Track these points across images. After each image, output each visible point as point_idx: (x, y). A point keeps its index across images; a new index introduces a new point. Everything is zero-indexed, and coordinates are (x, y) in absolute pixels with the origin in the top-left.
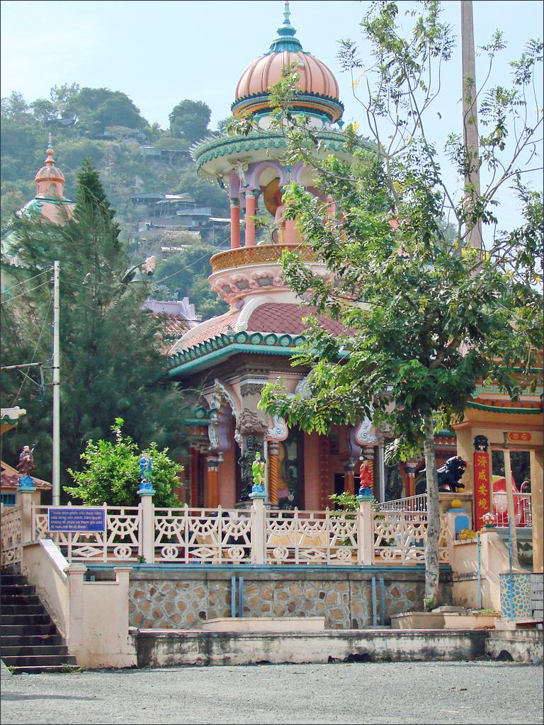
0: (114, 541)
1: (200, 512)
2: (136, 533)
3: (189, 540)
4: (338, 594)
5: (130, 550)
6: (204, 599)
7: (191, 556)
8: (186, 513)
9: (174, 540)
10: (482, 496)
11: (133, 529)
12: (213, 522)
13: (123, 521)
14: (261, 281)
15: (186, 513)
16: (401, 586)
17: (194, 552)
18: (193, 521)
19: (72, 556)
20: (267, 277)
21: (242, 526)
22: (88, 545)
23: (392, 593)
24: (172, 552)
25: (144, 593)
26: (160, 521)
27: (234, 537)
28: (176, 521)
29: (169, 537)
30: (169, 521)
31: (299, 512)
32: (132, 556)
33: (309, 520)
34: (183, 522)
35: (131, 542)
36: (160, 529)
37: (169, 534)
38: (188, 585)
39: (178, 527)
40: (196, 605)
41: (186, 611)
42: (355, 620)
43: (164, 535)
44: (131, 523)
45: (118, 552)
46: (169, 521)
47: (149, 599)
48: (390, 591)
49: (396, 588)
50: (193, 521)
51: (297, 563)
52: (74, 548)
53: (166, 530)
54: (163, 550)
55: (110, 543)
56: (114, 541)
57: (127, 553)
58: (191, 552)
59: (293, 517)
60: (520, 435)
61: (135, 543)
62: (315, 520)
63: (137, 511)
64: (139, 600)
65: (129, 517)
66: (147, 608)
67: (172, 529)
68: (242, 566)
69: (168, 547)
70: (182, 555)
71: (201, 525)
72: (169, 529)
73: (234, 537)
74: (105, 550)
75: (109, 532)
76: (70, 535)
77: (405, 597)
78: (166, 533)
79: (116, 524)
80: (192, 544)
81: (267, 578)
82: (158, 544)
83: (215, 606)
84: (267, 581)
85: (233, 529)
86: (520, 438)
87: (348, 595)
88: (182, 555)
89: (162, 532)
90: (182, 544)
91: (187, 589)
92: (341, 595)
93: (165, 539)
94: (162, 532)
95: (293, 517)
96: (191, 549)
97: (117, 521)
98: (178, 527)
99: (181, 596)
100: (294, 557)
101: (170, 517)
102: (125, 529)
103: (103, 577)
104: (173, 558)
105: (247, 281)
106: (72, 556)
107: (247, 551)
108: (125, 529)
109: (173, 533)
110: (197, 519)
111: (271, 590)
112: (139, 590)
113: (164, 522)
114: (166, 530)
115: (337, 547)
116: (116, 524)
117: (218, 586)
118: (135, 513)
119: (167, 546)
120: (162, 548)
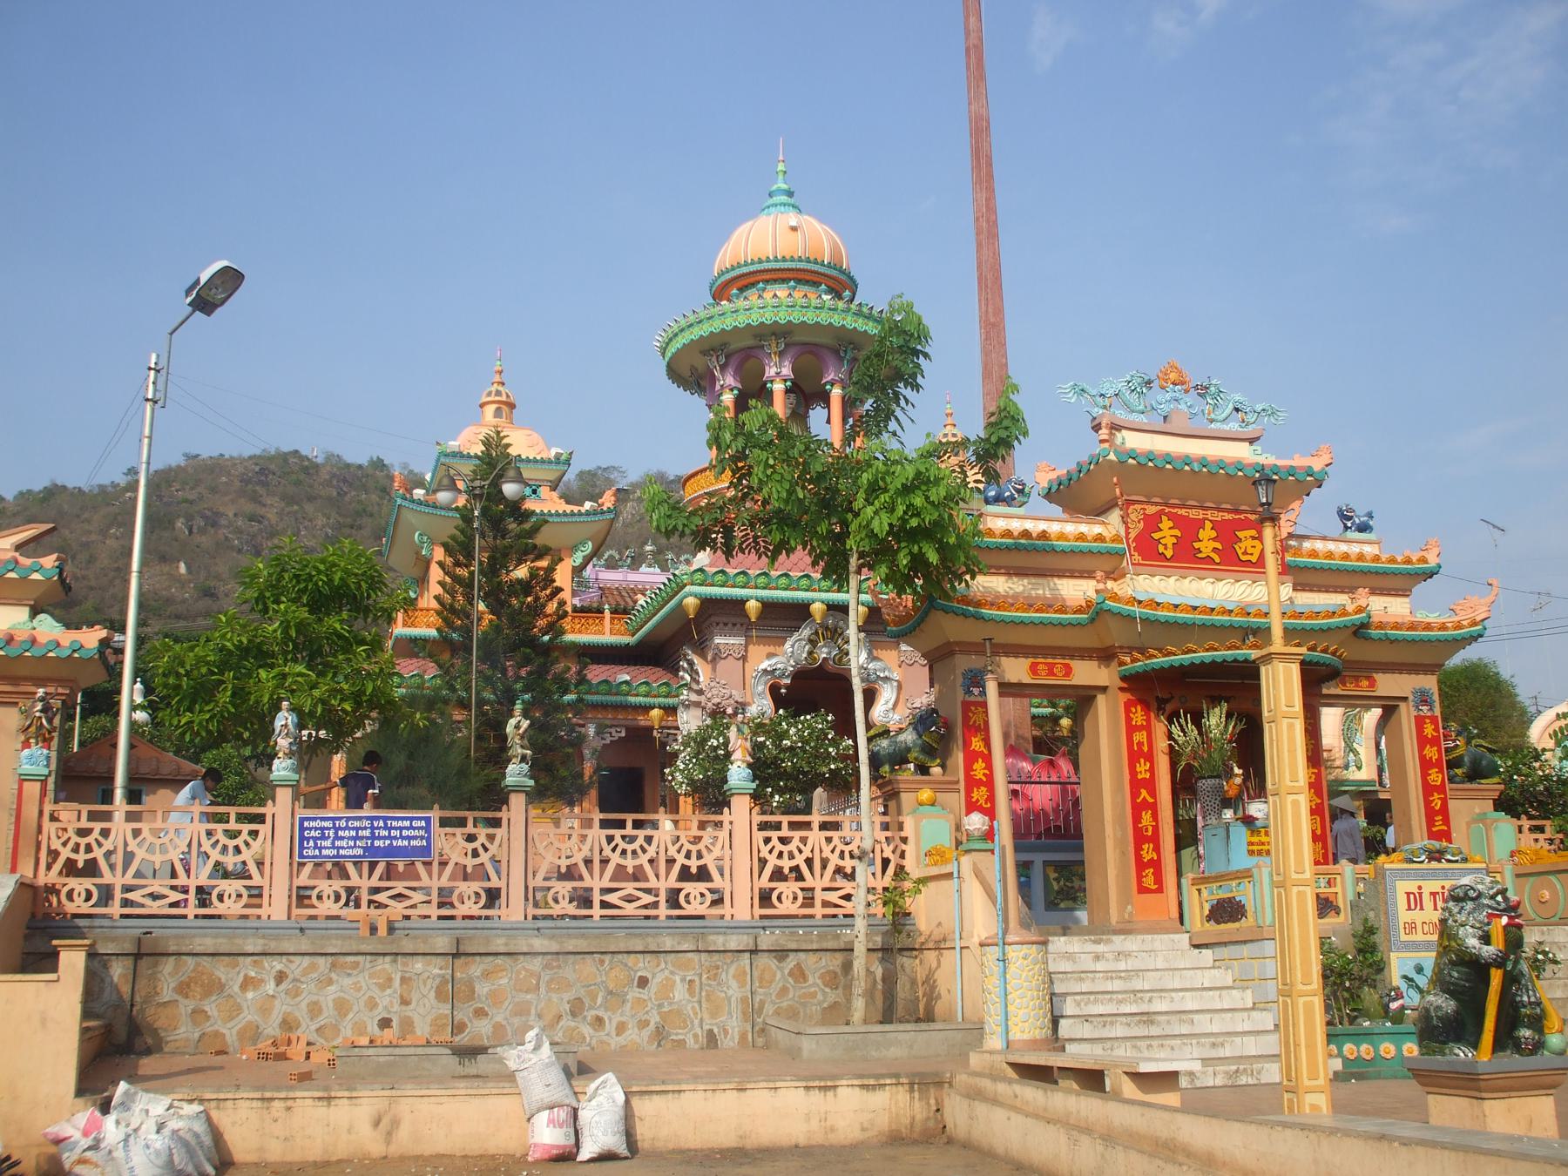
0: (771, 880)
1: (625, 821)
2: (495, 861)
3: (813, 875)
4: (677, 978)
5: (800, 895)
6: (389, 991)
7: (604, 905)
8: (816, 826)
9: (91, 869)
10: (979, 783)
11: (804, 856)
12: (804, 840)
13: (233, 835)
15: (816, 826)
16: (809, 961)
17: (612, 898)
18: (829, 840)
19: (602, 907)
21: (641, 847)
22: (630, 888)
23: (791, 974)
24: (332, 898)
25: (262, 981)
26: (829, 840)
27: (465, 866)
28: (245, 833)
29: (694, 870)
30: (783, 841)
31: (602, 816)
32: (803, 906)
33: (623, 832)
34: (589, 839)
35: (250, 877)
36: (768, 856)
37: (786, 864)
38: (357, 963)
39: (800, 851)
40: (372, 1004)
41: (351, 1015)
42: (710, 1032)
43: (68, 859)
44: (802, 846)
45: (779, 898)
46: (783, 841)
47: (271, 992)
48: (786, 972)
49: (798, 966)
50: (767, 840)
51: (819, 916)
52: (376, 890)
53: (688, 856)
54: (800, 900)
55: (672, 882)
56: (771, 880)
57: (795, 898)
58: (130, 896)
59: (500, 826)
60: (1051, 673)
61: (257, 880)
62: (635, 832)
63: (264, 815)
64: (250, 995)
65: (246, 828)
66: (265, 1011)
67: (89, 849)
68: (242, 923)
69: (788, 888)
70: (809, 902)
71: (79, 840)
72: (694, 855)
73: (465, 866)
74: (662, 898)
75: (54, 854)
76: (366, 868)
77: (819, 982)
78: (687, 862)
79: (218, 841)
80: (129, 879)
81: (525, 950)
82: (764, 881)
83: (412, 1007)
84: (525, 954)
85: (842, 852)
86: (1051, 673)
87: (697, 982)
88: (809, 902)
89: (773, 861)
90: (108, 879)
91: (355, 972)
92: (683, 980)
93: (778, 875)
94: (773, 861)
95: (500, 826)
96: (128, 889)
97: (775, 842)
98: (800, 851)
99: (342, 985)
100: (812, 905)
101: (629, 830)
102: (791, 856)
103: (173, 949)
104: (475, 910)
106: (602, 907)
107: (256, 894)
108: (700, 856)
109: (701, 862)
110: (774, 835)
111: (532, 974)
112: (253, 974)
113: (775, 842)
114: (688, 856)
115: (773, 885)
116: (218, 841)
117: (418, 965)
118: (260, 819)
119: (781, 886)
120: (680, 890)
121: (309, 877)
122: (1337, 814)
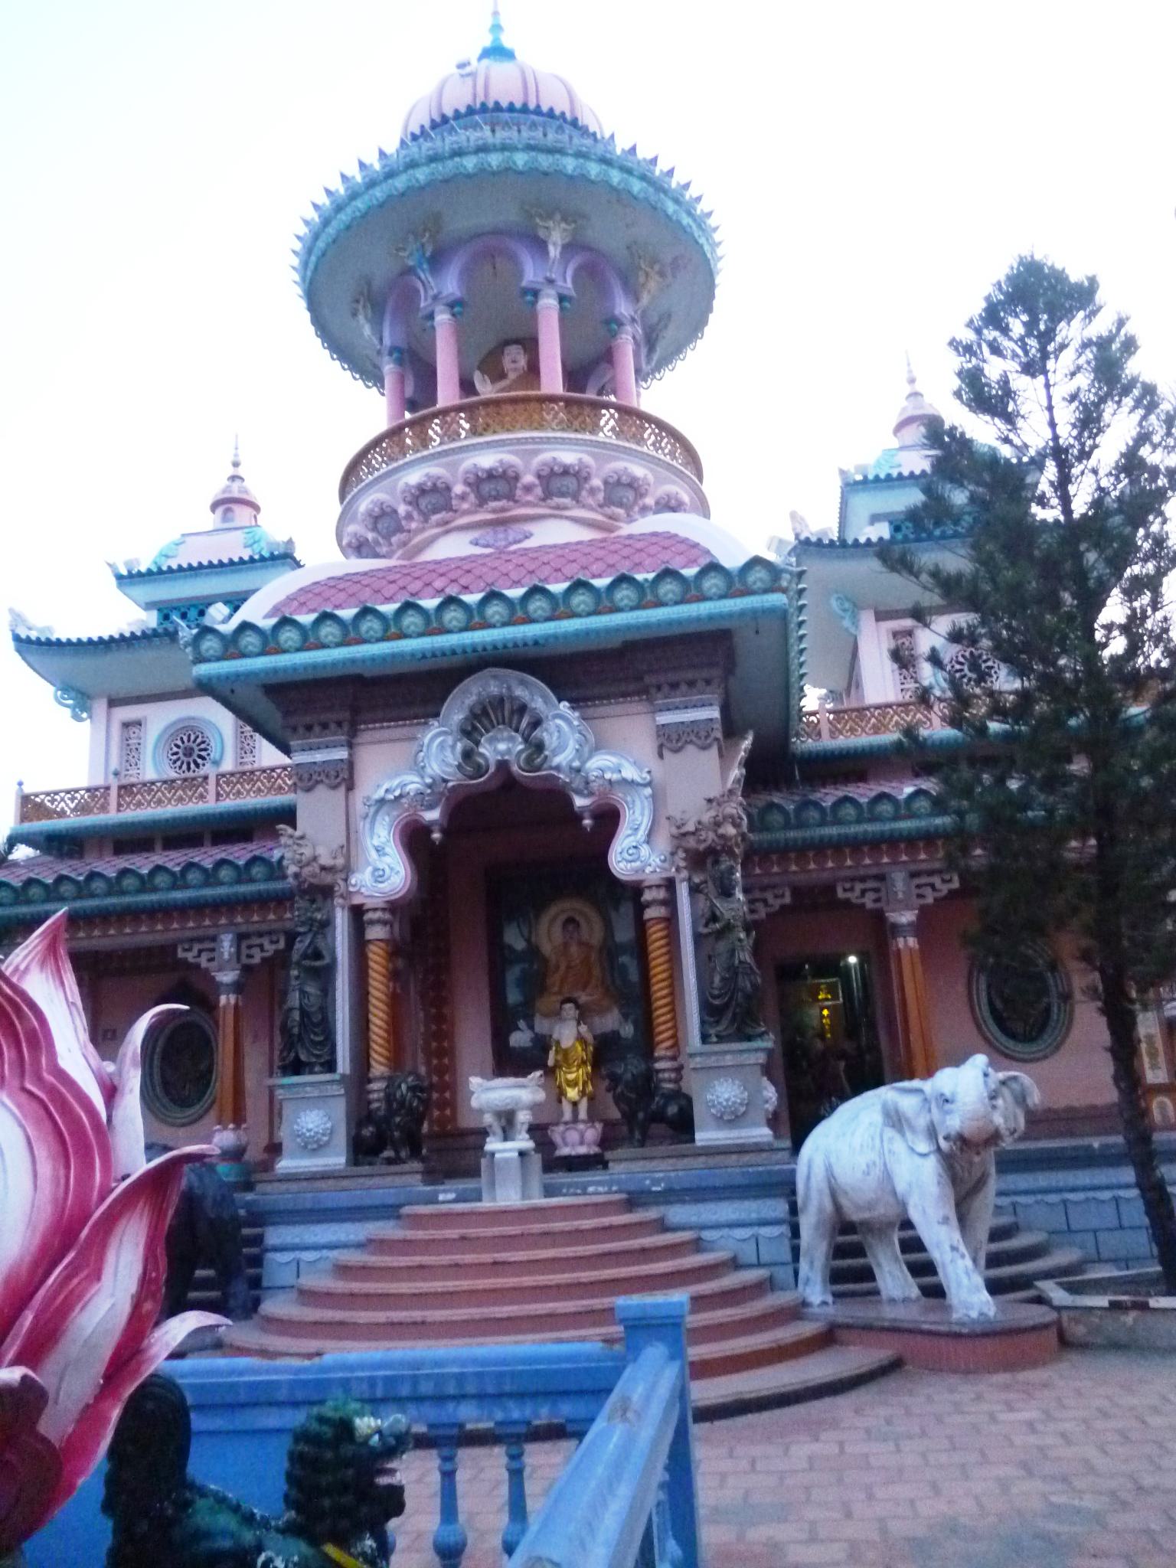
14: (486, 488)
20: (576, 475)
105: (395, 511)
121: (149, 1160)
122: (720, 935)
